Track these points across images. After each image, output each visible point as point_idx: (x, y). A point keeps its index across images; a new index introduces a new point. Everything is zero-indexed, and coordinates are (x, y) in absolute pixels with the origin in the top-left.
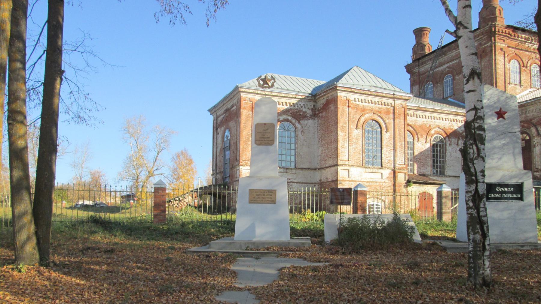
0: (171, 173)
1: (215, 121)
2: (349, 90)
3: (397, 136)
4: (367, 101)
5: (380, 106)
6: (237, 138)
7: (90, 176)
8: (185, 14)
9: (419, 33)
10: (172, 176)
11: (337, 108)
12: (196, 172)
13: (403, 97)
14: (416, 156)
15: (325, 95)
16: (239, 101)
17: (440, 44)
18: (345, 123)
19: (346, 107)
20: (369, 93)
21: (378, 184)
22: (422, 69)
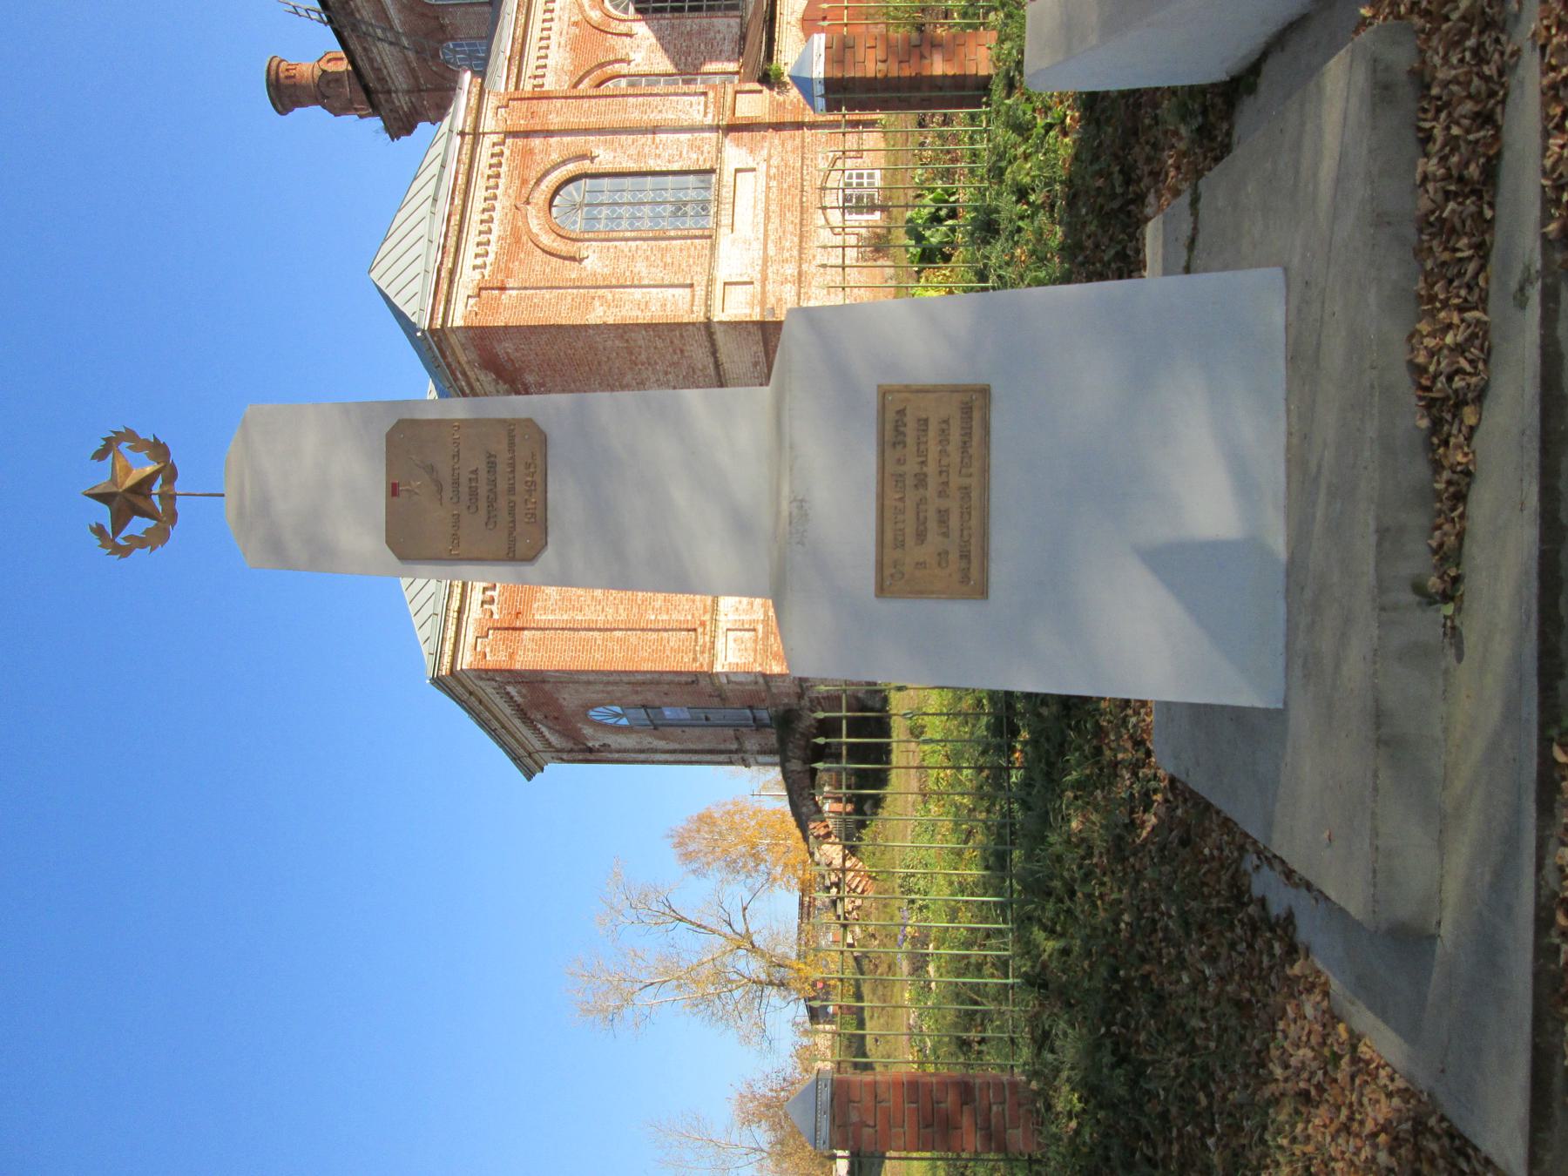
0: (742, 877)
1: (565, 756)
2: (444, 286)
3: (609, 120)
4: (484, 227)
5: (502, 182)
6: (616, 683)
7: (754, 1126)
9: (285, 93)
10: (749, 876)
11: (506, 327)
13: (473, 102)
14: (676, 65)
15: (464, 374)
16: (485, 674)
17: (315, 16)
18: (560, 298)
19: (505, 297)
20: (455, 219)
21: (773, 183)
22: (400, 80)
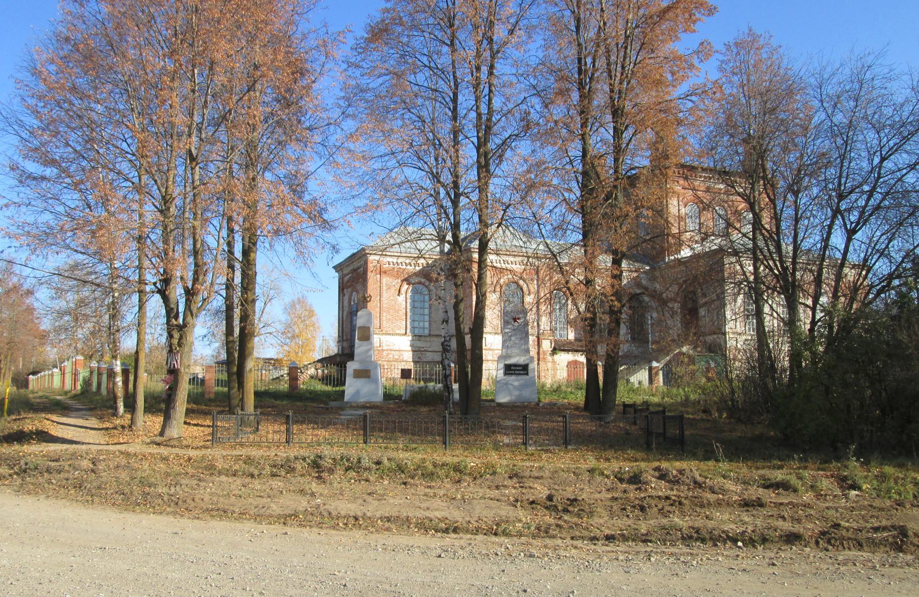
8: (313, 258)
12: (318, 328)
16: (366, 263)
